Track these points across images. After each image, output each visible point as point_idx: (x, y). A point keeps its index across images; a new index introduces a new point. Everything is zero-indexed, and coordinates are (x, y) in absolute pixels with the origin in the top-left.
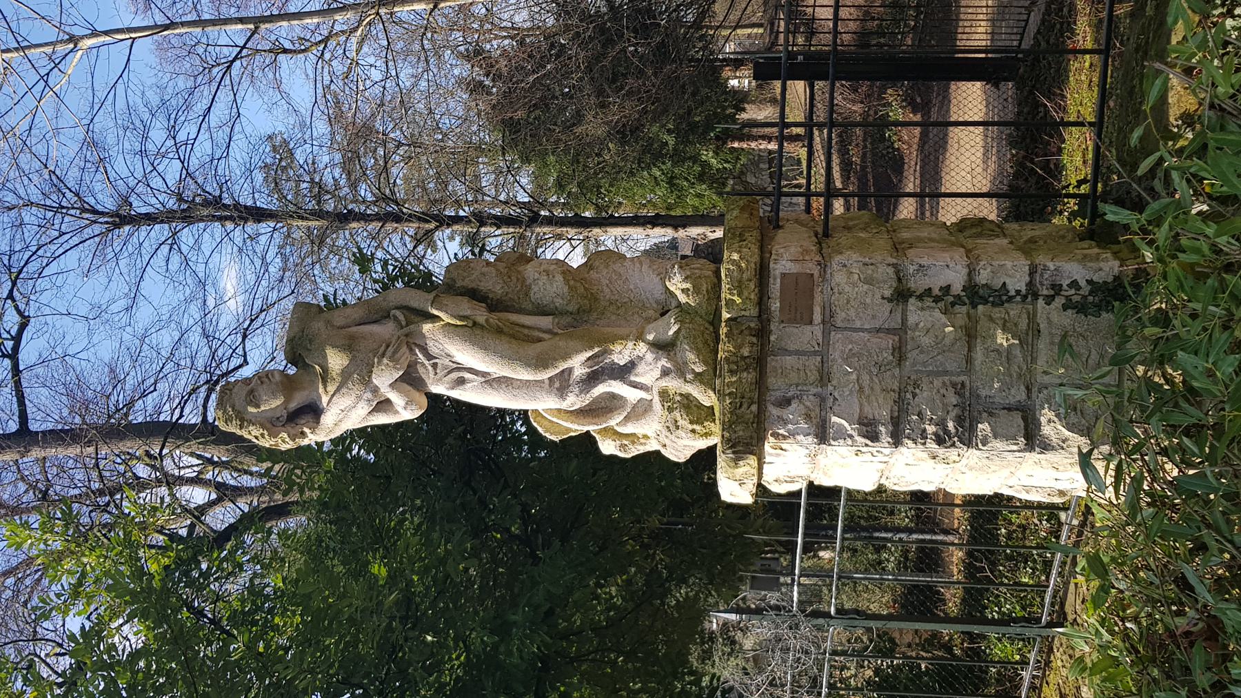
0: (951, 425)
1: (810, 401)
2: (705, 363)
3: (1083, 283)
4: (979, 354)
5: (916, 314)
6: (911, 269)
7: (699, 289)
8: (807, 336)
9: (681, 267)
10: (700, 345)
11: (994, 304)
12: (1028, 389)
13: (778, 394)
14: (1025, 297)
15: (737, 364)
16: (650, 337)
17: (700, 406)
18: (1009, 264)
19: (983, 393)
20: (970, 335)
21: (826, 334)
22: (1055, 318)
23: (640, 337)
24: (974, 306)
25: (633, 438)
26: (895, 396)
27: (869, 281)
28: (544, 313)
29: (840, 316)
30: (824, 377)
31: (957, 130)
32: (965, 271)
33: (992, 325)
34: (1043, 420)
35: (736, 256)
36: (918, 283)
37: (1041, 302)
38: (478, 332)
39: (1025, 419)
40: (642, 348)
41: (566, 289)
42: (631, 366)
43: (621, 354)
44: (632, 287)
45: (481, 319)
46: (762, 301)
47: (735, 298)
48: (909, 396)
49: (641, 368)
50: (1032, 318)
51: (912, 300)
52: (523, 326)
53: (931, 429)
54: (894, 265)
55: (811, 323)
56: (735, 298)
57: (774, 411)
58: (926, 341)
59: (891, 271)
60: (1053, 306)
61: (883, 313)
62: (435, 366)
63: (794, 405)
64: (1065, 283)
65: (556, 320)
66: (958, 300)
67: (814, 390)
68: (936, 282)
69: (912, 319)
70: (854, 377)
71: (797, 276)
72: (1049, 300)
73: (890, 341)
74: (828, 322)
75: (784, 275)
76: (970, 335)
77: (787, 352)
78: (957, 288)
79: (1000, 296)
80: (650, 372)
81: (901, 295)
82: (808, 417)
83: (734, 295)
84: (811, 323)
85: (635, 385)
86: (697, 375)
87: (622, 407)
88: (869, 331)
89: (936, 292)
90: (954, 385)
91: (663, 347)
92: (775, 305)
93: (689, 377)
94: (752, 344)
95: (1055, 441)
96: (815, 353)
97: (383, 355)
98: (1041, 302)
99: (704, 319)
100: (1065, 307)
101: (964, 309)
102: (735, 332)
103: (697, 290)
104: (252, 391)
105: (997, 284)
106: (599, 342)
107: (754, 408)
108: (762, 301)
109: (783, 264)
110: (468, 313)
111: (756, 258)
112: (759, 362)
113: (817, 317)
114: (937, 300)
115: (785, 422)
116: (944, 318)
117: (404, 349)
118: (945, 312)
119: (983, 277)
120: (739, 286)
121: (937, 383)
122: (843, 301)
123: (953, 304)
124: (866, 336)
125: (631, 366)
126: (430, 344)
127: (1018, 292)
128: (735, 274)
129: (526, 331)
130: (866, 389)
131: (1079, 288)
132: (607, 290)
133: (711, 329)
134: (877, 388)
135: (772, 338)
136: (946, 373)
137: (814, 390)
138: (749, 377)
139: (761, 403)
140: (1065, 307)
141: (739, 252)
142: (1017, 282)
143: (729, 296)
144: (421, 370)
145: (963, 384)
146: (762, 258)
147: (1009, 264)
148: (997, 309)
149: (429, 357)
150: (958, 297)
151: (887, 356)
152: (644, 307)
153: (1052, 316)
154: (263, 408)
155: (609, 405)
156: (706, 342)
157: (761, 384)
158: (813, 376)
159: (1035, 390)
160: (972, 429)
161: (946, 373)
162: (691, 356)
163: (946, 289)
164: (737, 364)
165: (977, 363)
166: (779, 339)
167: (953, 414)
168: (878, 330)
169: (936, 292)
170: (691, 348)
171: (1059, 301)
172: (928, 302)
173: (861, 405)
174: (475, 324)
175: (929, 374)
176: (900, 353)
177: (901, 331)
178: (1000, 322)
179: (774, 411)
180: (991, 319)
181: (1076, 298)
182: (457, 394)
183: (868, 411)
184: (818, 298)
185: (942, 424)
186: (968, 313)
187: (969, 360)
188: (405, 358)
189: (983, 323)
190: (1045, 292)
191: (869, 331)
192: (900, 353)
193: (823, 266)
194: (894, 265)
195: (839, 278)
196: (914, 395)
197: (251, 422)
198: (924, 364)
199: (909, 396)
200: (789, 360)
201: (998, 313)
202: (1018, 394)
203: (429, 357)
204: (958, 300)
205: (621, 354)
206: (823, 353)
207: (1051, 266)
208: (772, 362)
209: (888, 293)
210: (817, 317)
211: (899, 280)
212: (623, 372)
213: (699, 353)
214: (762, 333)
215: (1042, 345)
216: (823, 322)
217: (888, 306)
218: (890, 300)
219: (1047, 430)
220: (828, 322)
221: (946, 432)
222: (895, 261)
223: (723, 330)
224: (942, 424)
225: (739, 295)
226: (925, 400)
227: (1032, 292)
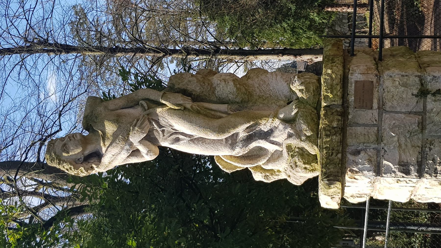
1: (371, 152)
2: (312, 130)
6: (429, 78)
7: (309, 90)
9: (298, 77)
10: (309, 121)
13: (353, 148)
16: (282, 116)
17: (309, 154)
21: (380, 115)
23: (276, 116)
25: (272, 172)
27: (405, 85)
29: (388, 105)
30: (379, 139)
35: (329, 71)
38: (186, 113)
40: (277, 122)
41: (235, 89)
42: (271, 132)
44: (271, 88)
45: (188, 106)
47: (329, 94)
48: (427, 149)
49: (276, 133)
51: (429, 96)
54: (419, 76)
55: (372, 108)
56: (329, 94)
57: (351, 158)
59: (417, 79)
62: (163, 131)
63: (362, 154)
65: (230, 107)
67: (373, 146)
69: (429, 106)
70: (396, 139)
74: (381, 108)
75: (356, 82)
77: (358, 125)
82: (370, 161)
83: (328, 93)
84: (372, 108)
85: (273, 143)
88: (405, 113)
91: (288, 122)
92: (352, 99)
94: (339, 120)
96: (374, 125)
97: (135, 125)
99: (312, 106)
102: (329, 113)
103: (307, 90)
104: (65, 145)
107: (340, 156)
110: (181, 102)
111: (341, 72)
113: (375, 105)
115: (357, 164)
117: (147, 122)
120: (331, 88)
124: (403, 116)
125: (271, 132)
126: (161, 119)
128: (329, 81)
129: (213, 113)
130: (403, 146)
132: (257, 90)
133: (316, 112)
134: (409, 145)
135: (350, 117)
137: (373, 146)
138: (336, 138)
139: (343, 153)
141: (331, 69)
143: (325, 94)
144: (155, 133)
146: (344, 73)
149: (160, 126)
151: (415, 127)
152: (278, 100)
154: (71, 154)
156: (312, 119)
157: (343, 142)
158: (373, 138)
162: (304, 127)
164: (330, 131)
168: (410, 113)
170: (304, 122)
174: (185, 108)
176: (422, 126)
177: (423, 113)
179: (351, 158)
184: (376, 95)
191: (405, 113)
192: (422, 126)
193: (379, 77)
194: (419, 76)
195: (388, 83)
196: (430, 149)
199: (427, 149)
200: (359, 129)
203: (160, 126)
206: (378, 125)
209: (415, 92)
210: (375, 105)
211: (422, 84)
214: (344, 114)
216: (379, 108)
217: (415, 99)
218: (417, 96)
220: (381, 108)
222: (419, 74)
223: (322, 112)
225: (331, 93)
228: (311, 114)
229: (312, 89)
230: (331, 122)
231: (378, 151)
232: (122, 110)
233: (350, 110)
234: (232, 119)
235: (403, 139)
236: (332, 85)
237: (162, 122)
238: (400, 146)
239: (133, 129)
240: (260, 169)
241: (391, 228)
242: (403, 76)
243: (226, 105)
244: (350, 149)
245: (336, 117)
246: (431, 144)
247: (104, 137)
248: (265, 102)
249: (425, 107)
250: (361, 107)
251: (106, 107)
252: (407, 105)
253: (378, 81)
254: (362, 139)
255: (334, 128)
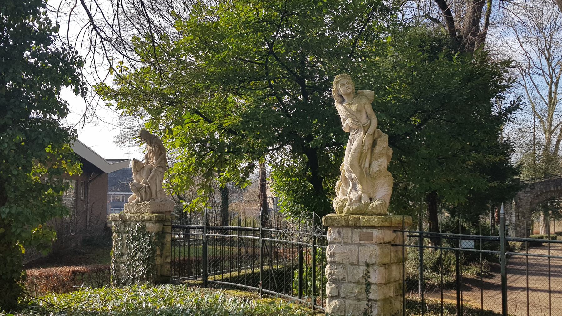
0: (334, 277)
1: (339, 240)
2: (353, 211)
3: (372, 314)
4: (352, 285)
5: (363, 268)
6: (375, 268)
8: (356, 239)
9: (381, 204)
11: (366, 290)
12: (344, 298)
13: (341, 231)
14: (368, 298)
15: (347, 220)
16: (363, 195)
17: (343, 209)
18: (377, 294)
19: (342, 286)
20: (358, 283)
21: (357, 244)
22: (362, 306)
23: (363, 192)
24: (365, 284)
25: (338, 191)
26: (341, 262)
27: (371, 256)
28: (370, 165)
29: (361, 248)
30: (346, 243)
31: (500, 296)
32: (374, 282)
33: (359, 289)
34: (336, 301)
35: (376, 220)
36: (371, 269)
37: (367, 302)
38: (361, 147)
39: (336, 296)
40: (360, 193)
42: (356, 190)
43: (359, 187)
45: (364, 148)
46: (364, 227)
48: (341, 266)
49: (355, 193)
50: (362, 300)
51: (366, 268)
52: (366, 159)
53: (333, 271)
54: (376, 263)
55: (360, 240)
57: (336, 230)
58: (355, 271)
59: (374, 262)
60: (366, 306)
61: (362, 260)
62: (354, 134)
63: (338, 235)
64: (372, 309)
66: (366, 280)
67: (342, 241)
68: (371, 274)
69: (361, 268)
70: (345, 251)
71: (373, 237)
72: (367, 305)
73: (355, 261)
74: (360, 245)
75: (373, 233)
76: (358, 283)
77: (352, 233)
78: (370, 280)
79: (368, 292)
80: (353, 196)
81: (368, 265)
82: (335, 239)
84: (360, 240)
85: (350, 191)
86: (350, 209)
87: (346, 187)
88: (358, 256)
89: (369, 274)
90: (344, 278)
91: (360, 198)
92: (364, 230)
93: (349, 207)
94: (352, 224)
95: (331, 304)
96: (352, 241)
97: (354, 121)
98: (367, 302)
100: (365, 309)
101: (364, 282)
103: (373, 209)
104: (344, 85)
105: (371, 291)
106: (360, 181)
107: (336, 225)
108: (364, 227)
109: (375, 232)
110: (366, 144)
111: (376, 225)
112: (348, 226)
113: (361, 242)
114: (366, 275)
115: (334, 233)
116: (361, 276)
117: (357, 127)
118: (363, 276)
119: (373, 287)
120: (368, 221)
121: (345, 274)
122: (365, 249)
123: (365, 279)
124: (357, 255)
125: (356, 190)
126: (359, 133)
127: (369, 296)
130: (342, 255)
131: (370, 313)
134: (343, 258)
135: (356, 230)
136: (348, 276)
137: (342, 241)
138: (344, 223)
139: (337, 226)
140: (365, 309)
142: (371, 296)
144: (353, 131)
145: (344, 280)
146: (376, 227)
147: (377, 294)
148: (364, 290)
149: (356, 133)
150: (367, 280)
151: (351, 261)
152: (373, 193)
153: (363, 305)
155: (347, 184)
156: (359, 211)
157: (342, 226)
158: (346, 241)
159: (344, 299)
160: (333, 282)
161: (348, 276)
162: (354, 207)
163: (369, 277)
164: (347, 220)
165: (350, 284)
166: (356, 232)
167: (337, 277)
168: (358, 258)
169: (369, 274)
171: (367, 307)
172: (365, 272)
173: (338, 253)
174: (363, 146)
175: (347, 272)
176: (352, 264)
177: (358, 265)
178: (360, 291)
179: (336, 230)
180: (361, 289)
181: (368, 312)
182: (73, 268)
183: (337, 255)
184: (367, 242)
185: (334, 274)
186: (363, 283)
187: (351, 282)
188: (355, 127)
189: (360, 286)
190: (369, 304)
191: (358, 256)
192: (352, 264)
193: (375, 244)
194: (376, 263)
195: (372, 248)
196: (341, 267)
197: (336, 85)
198: (350, 270)
199: (341, 266)
200: (350, 234)
201: (363, 290)
202: (342, 295)
203: (356, 133)
204: (366, 280)
205: (359, 187)
206: (352, 243)
207: (377, 306)
208: (349, 230)
209: (367, 261)
210: (361, 242)
211: (372, 264)
212: (354, 188)
213: (355, 209)
214: (356, 227)
215: (356, 302)
216: (360, 244)
217: (364, 261)
218: (366, 262)
219: (333, 301)
220: (360, 245)
221: (332, 275)
222: (377, 263)
223: (357, 216)
224: (334, 274)
226: (340, 270)
227: (369, 300)
228: (361, 210)
229: (374, 211)
230: (351, 221)
231: (340, 243)
232: (365, 113)
233: (359, 230)
234: (358, 171)
235: (345, 255)
236: (369, 221)
237: (358, 134)
238: (342, 253)
239: (352, 120)
240: (340, 185)
241: (480, 254)
242: (376, 255)
243: (368, 166)
244: (341, 230)
245: (354, 223)
246: (344, 268)
247: (350, 104)
248: (372, 186)
249: (361, 265)
250: (360, 235)
251: (365, 104)
252: (361, 257)
253: (373, 243)
254: (345, 235)
255: (348, 222)
